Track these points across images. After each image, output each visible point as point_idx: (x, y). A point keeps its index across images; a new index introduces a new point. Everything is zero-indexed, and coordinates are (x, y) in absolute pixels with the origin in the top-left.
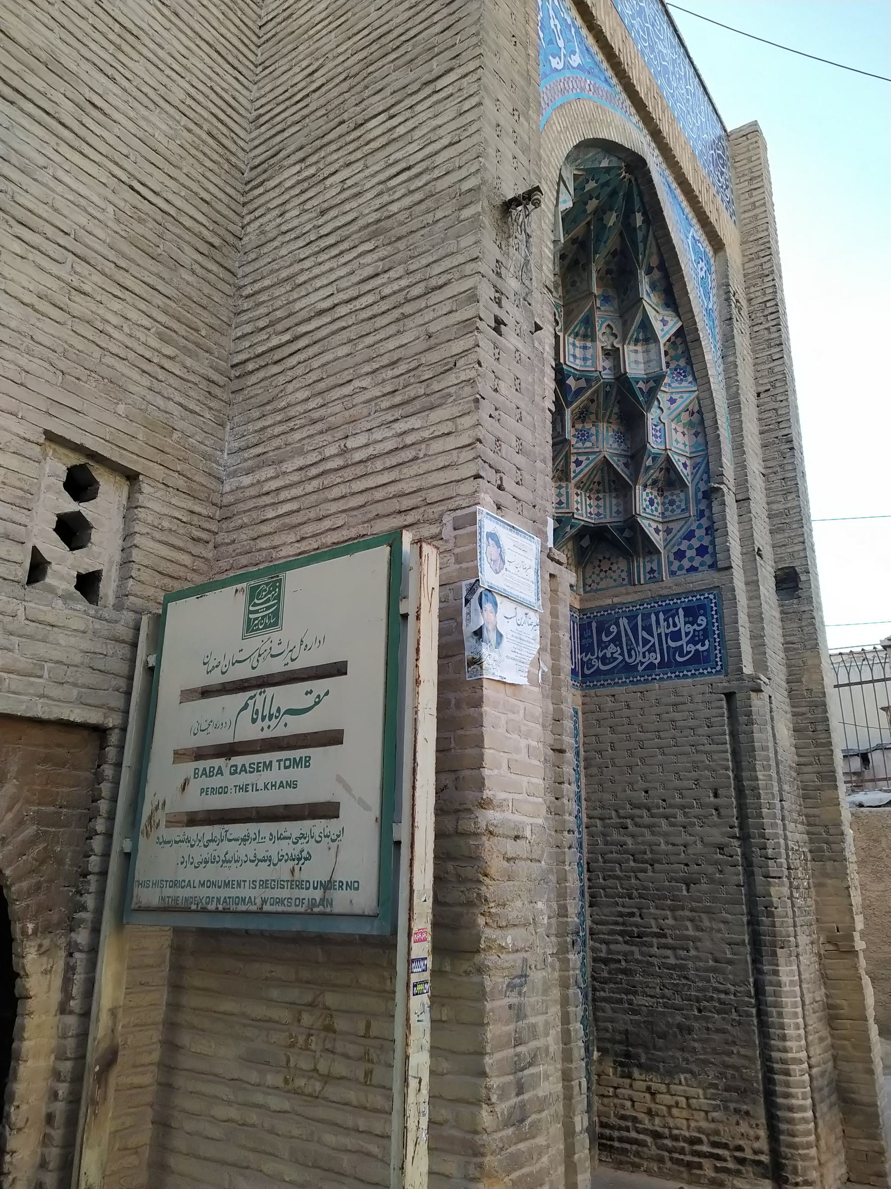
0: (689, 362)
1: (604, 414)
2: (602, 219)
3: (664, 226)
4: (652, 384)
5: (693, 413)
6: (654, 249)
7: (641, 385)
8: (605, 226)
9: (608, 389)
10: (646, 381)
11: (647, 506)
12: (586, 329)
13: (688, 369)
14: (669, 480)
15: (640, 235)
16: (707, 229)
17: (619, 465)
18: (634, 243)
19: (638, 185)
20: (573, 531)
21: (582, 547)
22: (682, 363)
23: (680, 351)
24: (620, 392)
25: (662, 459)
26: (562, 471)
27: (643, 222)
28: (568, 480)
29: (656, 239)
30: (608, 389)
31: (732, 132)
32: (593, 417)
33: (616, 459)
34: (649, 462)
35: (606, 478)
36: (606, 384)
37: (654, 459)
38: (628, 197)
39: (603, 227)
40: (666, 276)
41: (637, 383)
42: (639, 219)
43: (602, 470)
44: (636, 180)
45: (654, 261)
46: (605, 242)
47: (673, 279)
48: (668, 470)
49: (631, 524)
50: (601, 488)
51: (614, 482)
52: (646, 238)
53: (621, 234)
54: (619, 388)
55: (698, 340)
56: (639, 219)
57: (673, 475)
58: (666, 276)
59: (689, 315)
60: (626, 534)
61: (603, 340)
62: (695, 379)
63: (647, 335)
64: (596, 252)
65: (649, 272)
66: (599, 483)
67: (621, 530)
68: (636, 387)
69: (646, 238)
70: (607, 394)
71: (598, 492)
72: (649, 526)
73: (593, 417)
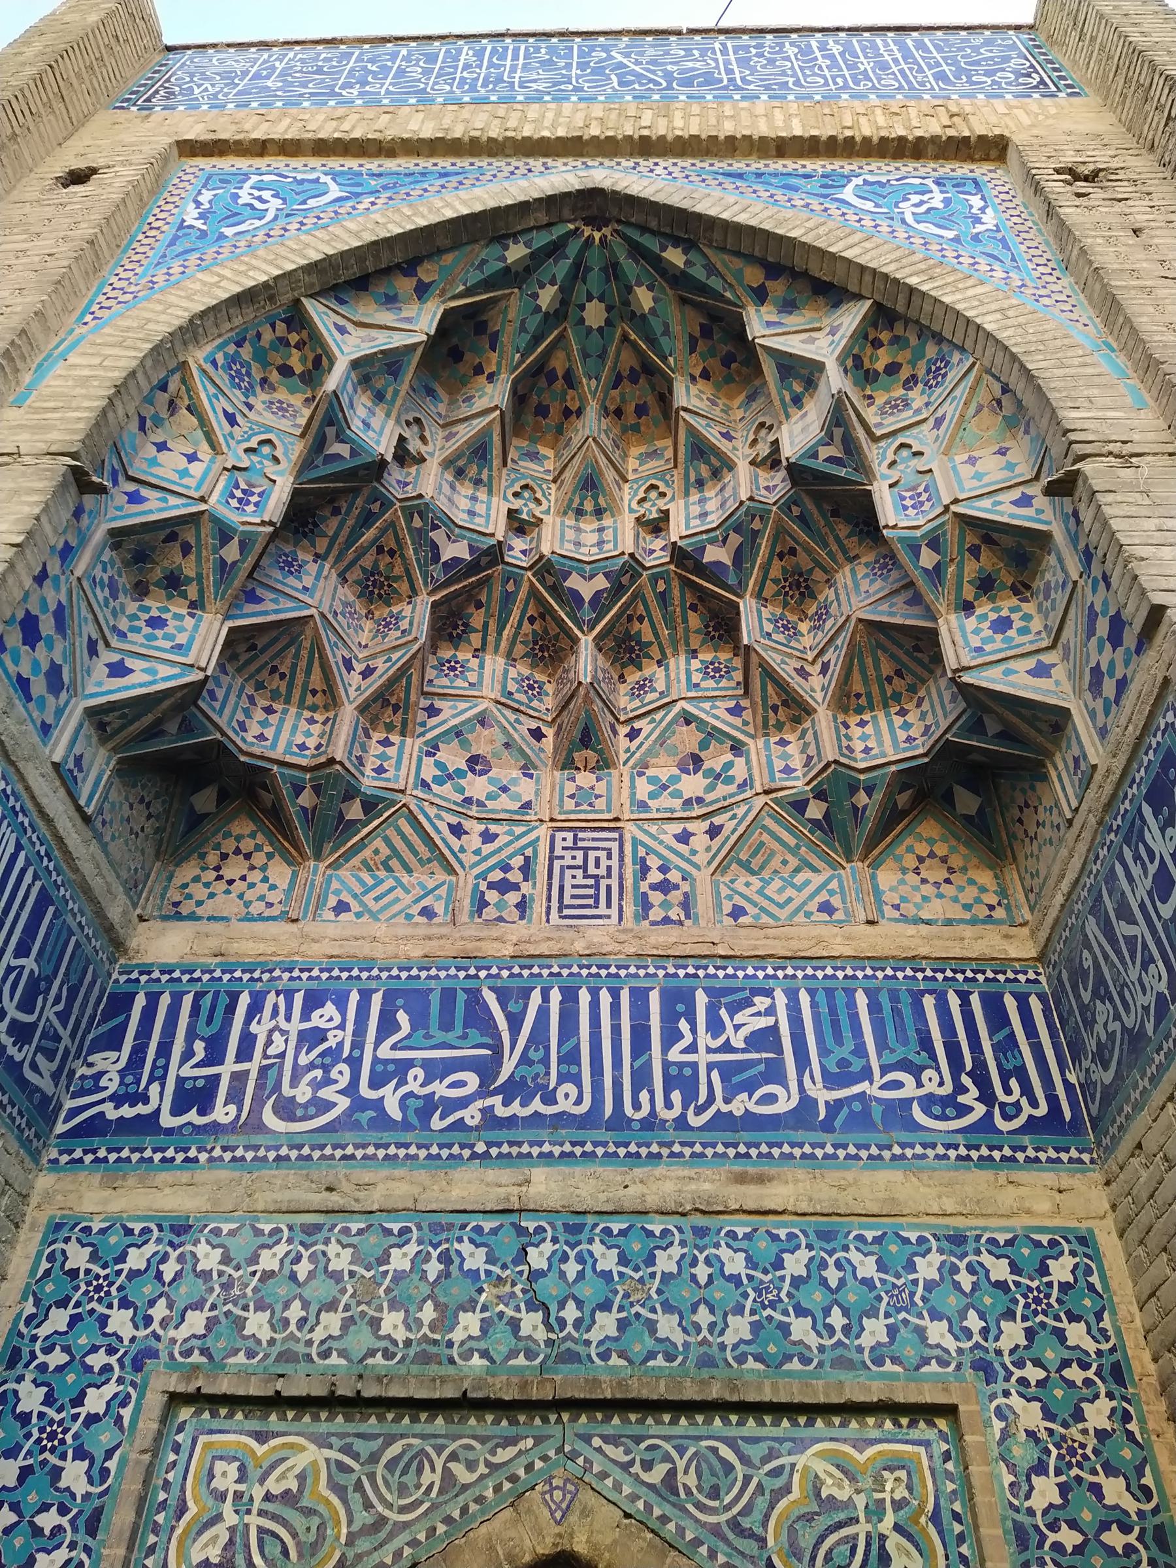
0: (938, 338)
1: (831, 554)
2: (633, 313)
3: (711, 223)
4: (838, 433)
5: (999, 402)
6: (737, 263)
7: (824, 452)
8: (643, 316)
9: (796, 511)
10: (828, 440)
11: (990, 648)
12: (708, 463)
13: (945, 348)
14: (1006, 557)
15: (698, 272)
16: (930, 149)
17: (898, 614)
18: (703, 289)
19: (628, 224)
20: (878, 796)
21: (968, 819)
22: (931, 350)
23: (914, 341)
24: (818, 498)
25: (952, 534)
26: (785, 703)
27: (685, 252)
28: (809, 711)
29: (723, 249)
30: (796, 511)
31: (1042, 13)
32: (818, 575)
33: (885, 607)
34: (928, 558)
35: (900, 653)
36: (787, 506)
37: (934, 544)
38: (638, 251)
39: (639, 320)
40: (796, 275)
41: (815, 456)
42: (675, 257)
43: (879, 646)
44: (619, 221)
45: (754, 276)
46: (666, 332)
47: (799, 263)
48: (988, 540)
49: (980, 703)
50: (909, 679)
51: (917, 648)
52: (711, 269)
53: (683, 301)
54: (808, 492)
55: (912, 290)
56: (675, 257)
57: (1007, 541)
58: (796, 275)
59: (868, 278)
60: (992, 727)
61: (741, 453)
62: (962, 349)
63: (801, 373)
64: (664, 359)
65: (760, 295)
66: (899, 673)
67: (976, 727)
68: (819, 464)
69: (711, 269)
70: (803, 520)
71: (913, 689)
72: (1015, 681)
73: (818, 575)
